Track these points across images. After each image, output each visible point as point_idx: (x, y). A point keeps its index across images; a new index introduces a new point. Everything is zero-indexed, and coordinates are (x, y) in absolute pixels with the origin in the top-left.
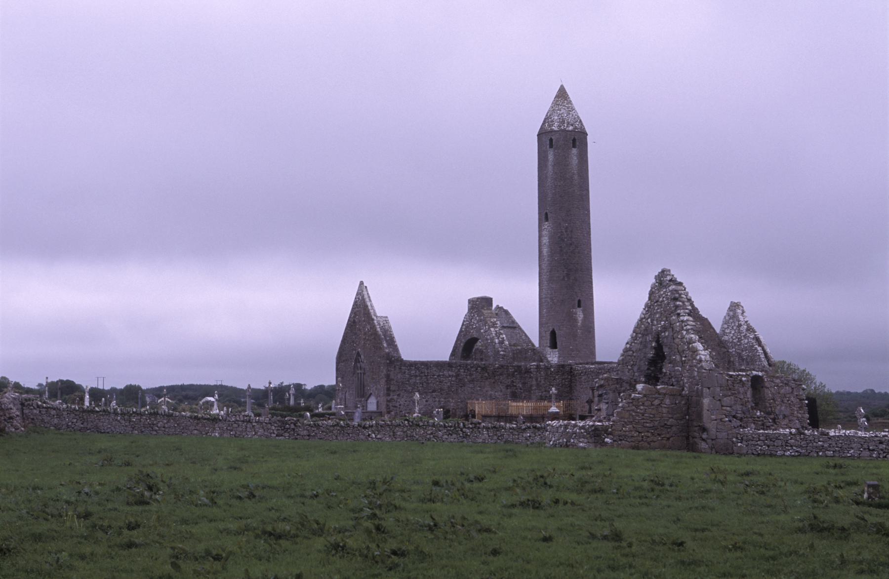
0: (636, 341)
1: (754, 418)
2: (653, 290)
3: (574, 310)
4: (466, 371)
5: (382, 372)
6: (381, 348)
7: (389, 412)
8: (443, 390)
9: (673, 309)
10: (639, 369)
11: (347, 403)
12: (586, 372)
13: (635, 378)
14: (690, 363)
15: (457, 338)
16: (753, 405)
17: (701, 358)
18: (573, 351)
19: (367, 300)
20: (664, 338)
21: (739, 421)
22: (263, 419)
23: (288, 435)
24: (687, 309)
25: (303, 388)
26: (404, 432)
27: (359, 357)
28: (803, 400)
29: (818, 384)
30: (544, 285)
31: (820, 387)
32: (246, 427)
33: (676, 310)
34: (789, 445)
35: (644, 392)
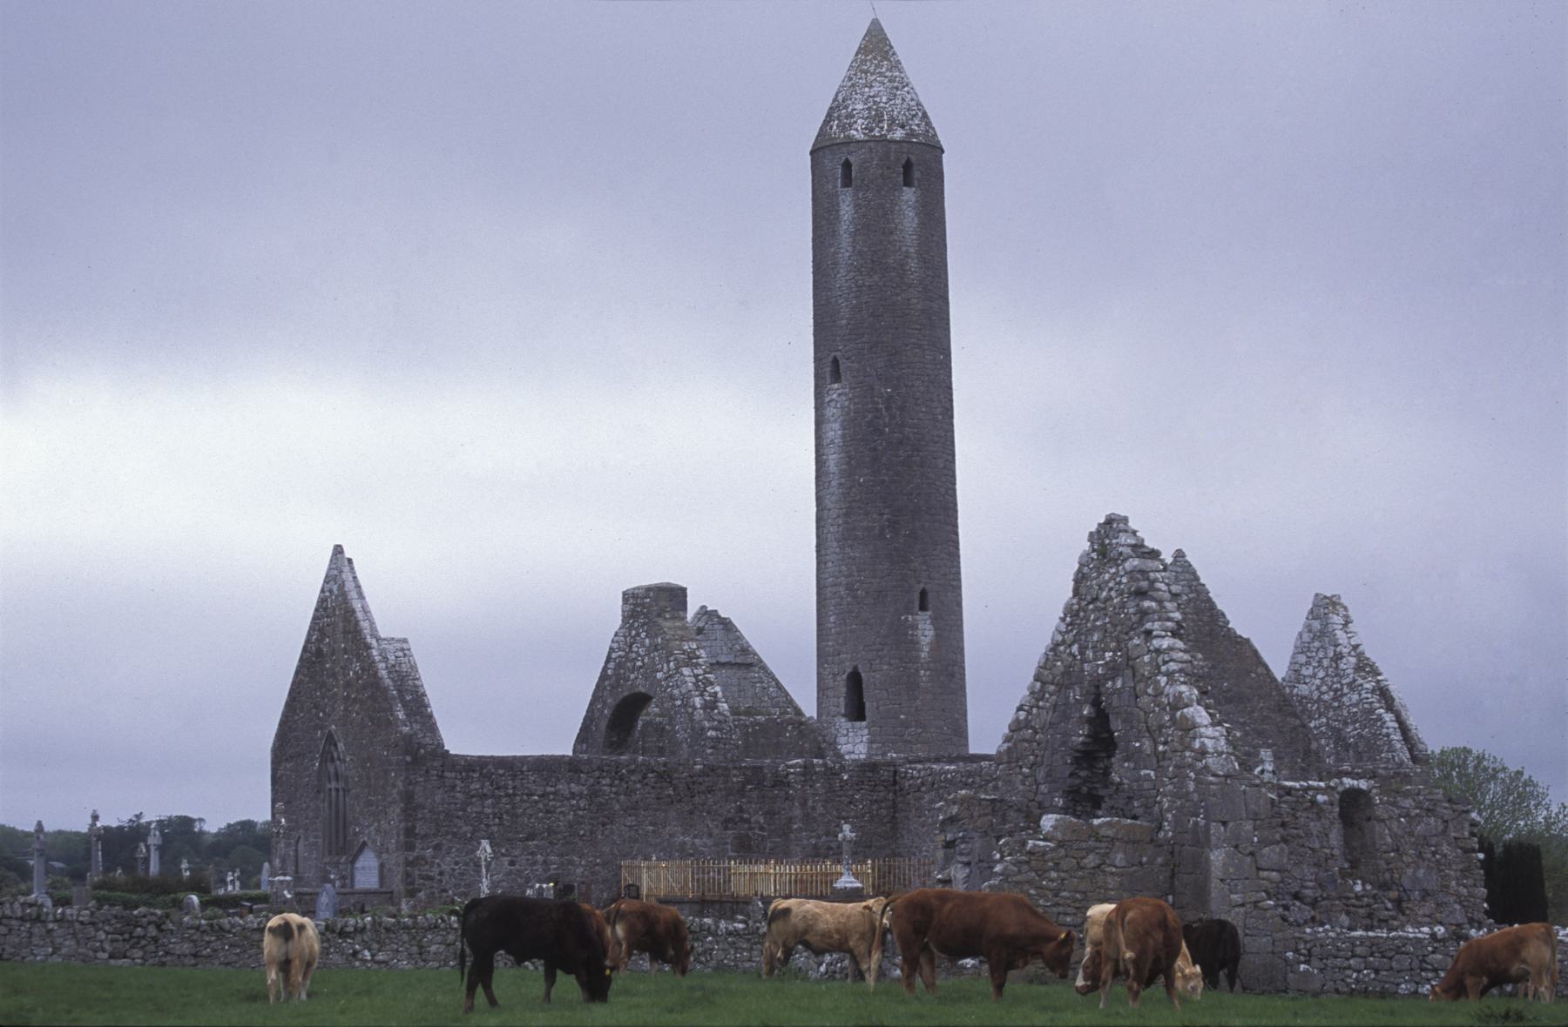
0: (1041, 704)
1: (1348, 898)
2: (1086, 570)
3: (910, 618)
4: (617, 782)
5: (394, 786)
6: (390, 724)
7: (411, 894)
8: (557, 833)
9: (1134, 619)
10: (1048, 775)
11: (300, 870)
12: (933, 784)
13: (1039, 798)
14: (1176, 759)
15: (594, 695)
16: (1346, 865)
17: (1203, 744)
18: (907, 728)
19: (353, 594)
20: (1113, 694)
21: (1307, 907)
22: (75, 912)
23: (140, 954)
24: (1169, 619)
25: (196, 830)
26: (449, 945)
27: (332, 748)
28: (1474, 851)
29: (1555, 809)
30: (829, 552)
31: (1561, 817)
32: (31, 935)
33: (1141, 622)
34: (1430, 967)
35: (1059, 835)
